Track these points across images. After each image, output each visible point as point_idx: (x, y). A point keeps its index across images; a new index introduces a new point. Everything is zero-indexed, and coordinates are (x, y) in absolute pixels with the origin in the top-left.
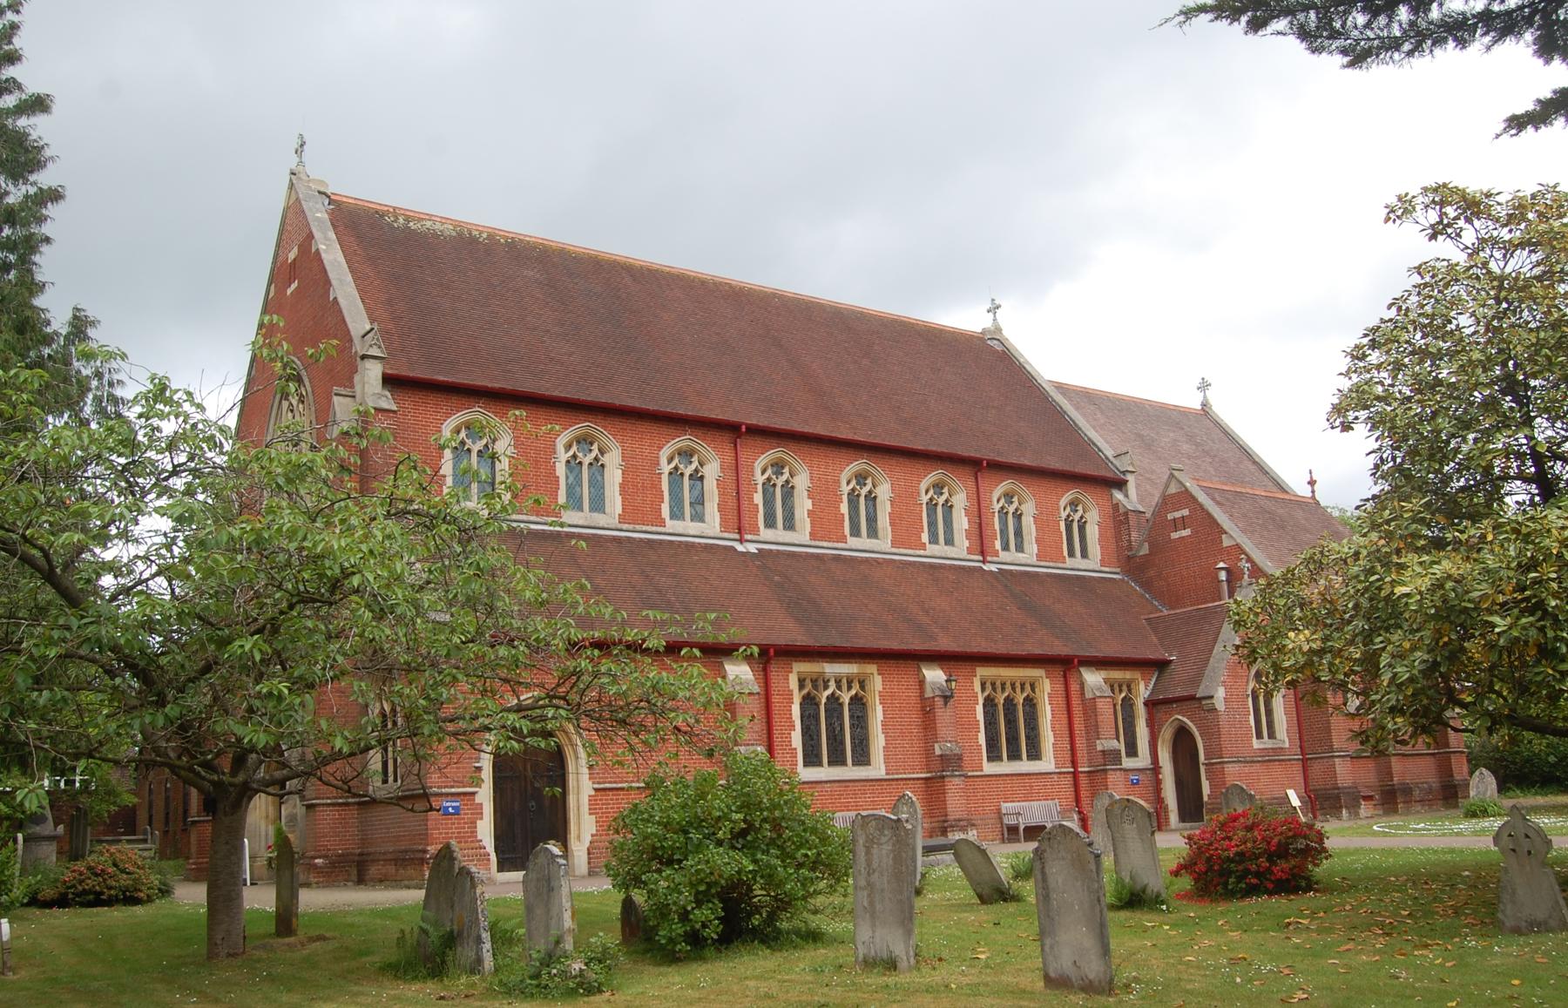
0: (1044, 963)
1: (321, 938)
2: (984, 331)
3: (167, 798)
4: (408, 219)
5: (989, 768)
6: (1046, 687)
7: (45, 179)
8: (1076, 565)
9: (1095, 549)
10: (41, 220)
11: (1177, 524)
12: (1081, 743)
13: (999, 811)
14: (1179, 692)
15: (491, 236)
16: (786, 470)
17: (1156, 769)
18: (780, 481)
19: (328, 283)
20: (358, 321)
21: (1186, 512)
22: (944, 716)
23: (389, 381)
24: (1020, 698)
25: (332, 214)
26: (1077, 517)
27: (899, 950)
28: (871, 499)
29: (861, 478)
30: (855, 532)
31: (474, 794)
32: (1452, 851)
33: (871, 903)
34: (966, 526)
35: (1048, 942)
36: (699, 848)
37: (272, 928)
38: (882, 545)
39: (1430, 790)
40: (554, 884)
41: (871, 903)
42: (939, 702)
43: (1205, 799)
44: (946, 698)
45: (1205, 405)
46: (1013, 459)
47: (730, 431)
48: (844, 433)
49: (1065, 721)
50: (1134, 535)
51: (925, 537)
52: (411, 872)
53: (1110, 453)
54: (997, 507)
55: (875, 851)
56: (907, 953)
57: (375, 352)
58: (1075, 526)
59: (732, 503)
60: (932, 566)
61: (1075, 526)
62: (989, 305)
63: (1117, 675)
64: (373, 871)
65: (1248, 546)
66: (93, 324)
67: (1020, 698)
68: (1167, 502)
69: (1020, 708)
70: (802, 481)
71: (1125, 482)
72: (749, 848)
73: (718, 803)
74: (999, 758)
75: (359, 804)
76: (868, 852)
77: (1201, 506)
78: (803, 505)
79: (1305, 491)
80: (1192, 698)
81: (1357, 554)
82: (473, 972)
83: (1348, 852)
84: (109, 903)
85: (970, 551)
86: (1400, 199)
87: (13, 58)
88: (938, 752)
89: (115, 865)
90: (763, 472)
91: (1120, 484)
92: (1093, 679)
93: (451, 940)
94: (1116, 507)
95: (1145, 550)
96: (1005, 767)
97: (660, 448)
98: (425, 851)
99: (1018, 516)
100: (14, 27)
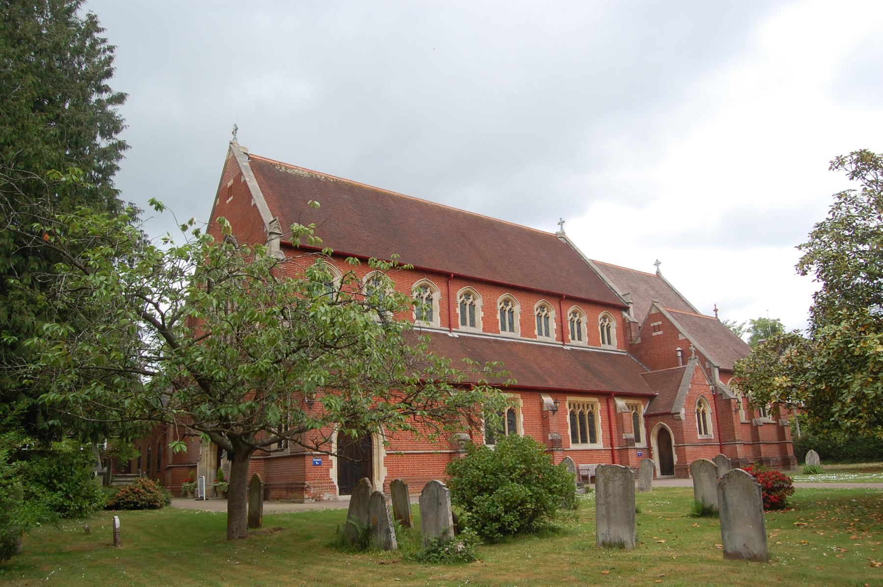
0: (724, 545)
1: (280, 529)
2: (557, 234)
3: (149, 455)
4: (286, 168)
5: (573, 447)
6: (599, 407)
7: (119, 137)
8: (606, 348)
9: (614, 340)
10: (119, 157)
11: (655, 329)
12: (615, 435)
13: (578, 468)
14: (661, 411)
15: (326, 178)
16: (471, 297)
17: (649, 448)
18: (468, 302)
19: (251, 196)
20: (267, 216)
21: (660, 323)
22: (553, 420)
23: (284, 246)
24: (587, 412)
25: (250, 163)
26: (606, 324)
27: (626, 537)
28: (511, 312)
29: (506, 302)
30: (504, 329)
32: (826, 490)
33: (608, 513)
34: (555, 327)
35: (727, 533)
36: (503, 483)
38: (516, 335)
39: (777, 461)
40: (442, 501)
41: (608, 513)
42: (550, 413)
43: (675, 463)
44: (554, 411)
45: (658, 272)
46: (577, 295)
47: (445, 277)
48: (499, 280)
49: (607, 424)
50: (633, 333)
51: (536, 332)
52: (296, 494)
53: (620, 294)
54: (569, 318)
55: (611, 484)
56: (632, 540)
57: (277, 231)
58: (605, 328)
59: (446, 312)
60: (540, 346)
61: (605, 328)
62: (559, 221)
63: (631, 401)
64: (273, 493)
65: (691, 339)
66: (139, 211)
67: (587, 412)
68: (650, 318)
69: (587, 417)
70: (479, 303)
71: (629, 308)
72: (527, 483)
73: (509, 459)
74: (577, 442)
75: (265, 459)
76: (606, 485)
77: (668, 320)
78: (479, 314)
80: (669, 414)
81: (834, 334)
82: (386, 549)
83: (801, 489)
84: (141, 508)
85: (557, 339)
86: (838, 158)
87: (109, 74)
88: (550, 438)
89: (144, 488)
90: (461, 297)
91: (626, 309)
92: (621, 403)
93: (369, 532)
94: (624, 320)
95: (639, 341)
96: (580, 446)
97: (412, 284)
98: (304, 484)
99: (579, 323)
100: (111, 58)
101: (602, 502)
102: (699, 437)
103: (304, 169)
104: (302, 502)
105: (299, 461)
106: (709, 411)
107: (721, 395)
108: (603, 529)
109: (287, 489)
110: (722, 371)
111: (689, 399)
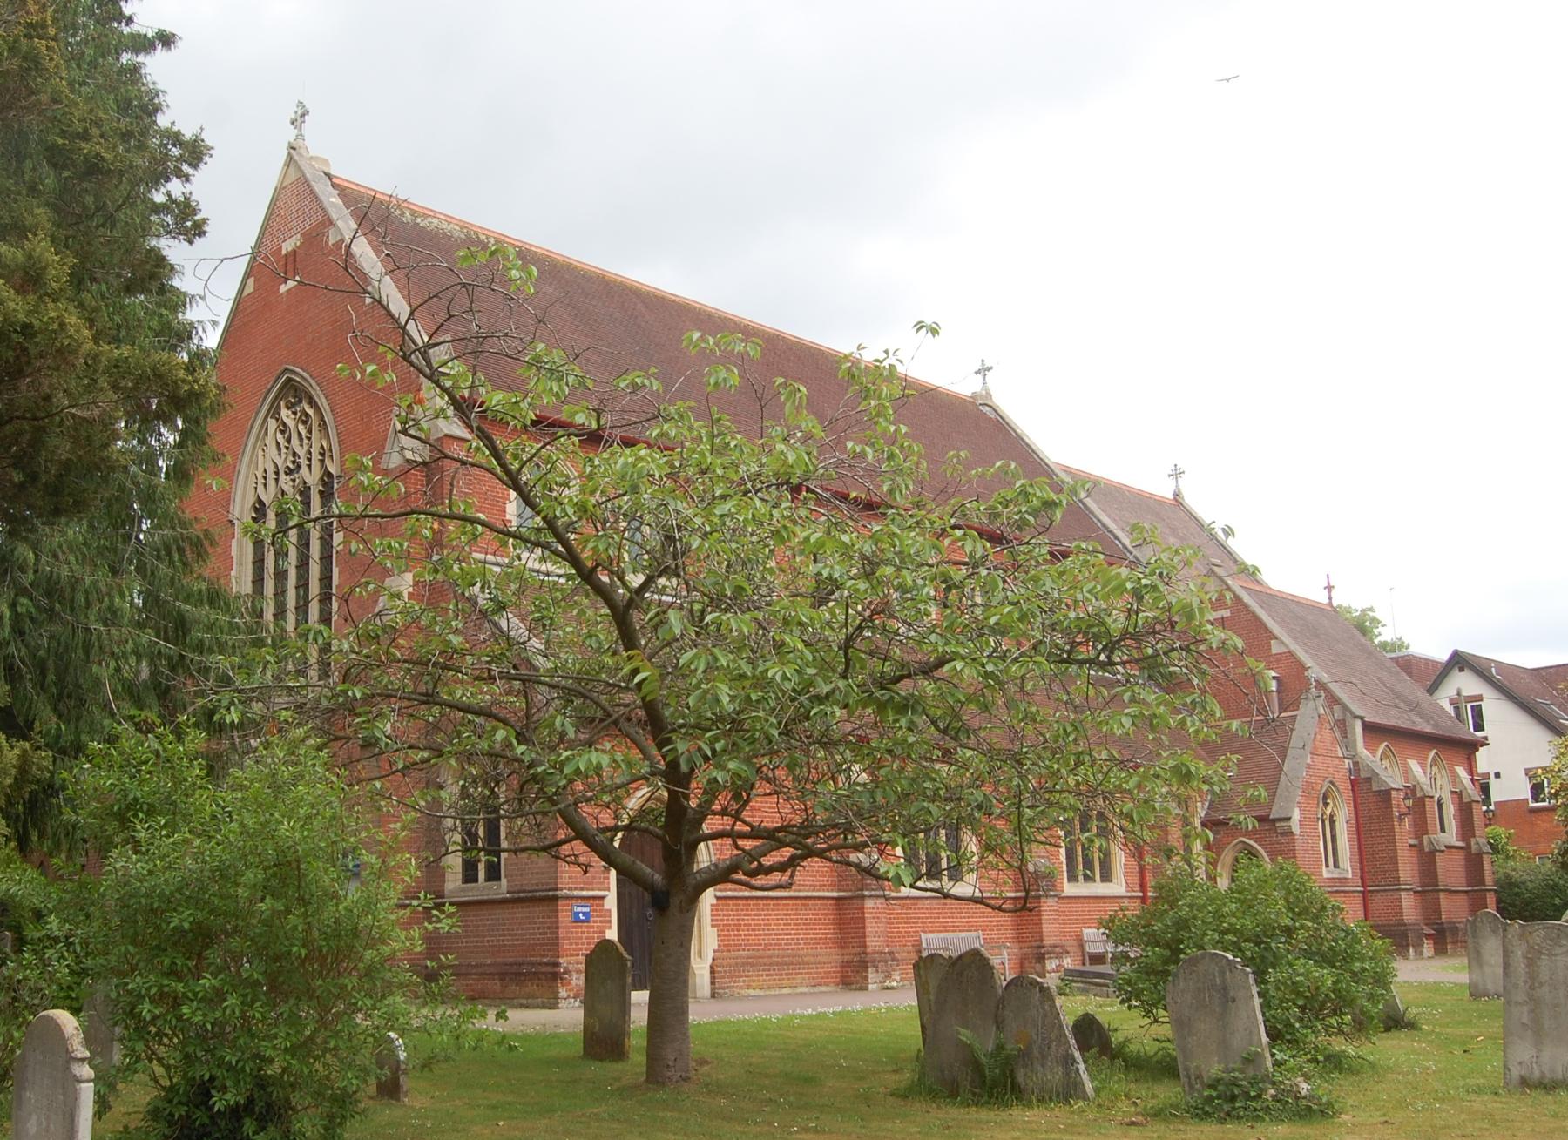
2: (974, 396)
4: (413, 213)
5: (1069, 889)
31: (602, 898)
37: (579, 1048)
45: (1177, 495)
55: (1544, 962)
62: (978, 366)
76: (1531, 963)
77: (1246, 607)
79: (1322, 598)
98: (557, 965)
101: (1520, 996)
102: (1326, 875)
103: (450, 219)
104: (554, 1006)
105: (538, 912)
106: (1343, 814)
107: (1368, 780)
108: (1523, 1052)
109: (502, 976)
110: (1371, 729)
111: (1307, 791)
